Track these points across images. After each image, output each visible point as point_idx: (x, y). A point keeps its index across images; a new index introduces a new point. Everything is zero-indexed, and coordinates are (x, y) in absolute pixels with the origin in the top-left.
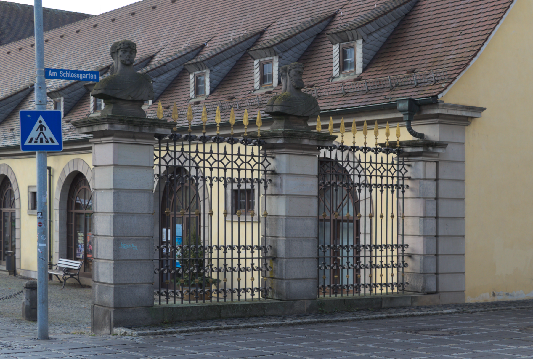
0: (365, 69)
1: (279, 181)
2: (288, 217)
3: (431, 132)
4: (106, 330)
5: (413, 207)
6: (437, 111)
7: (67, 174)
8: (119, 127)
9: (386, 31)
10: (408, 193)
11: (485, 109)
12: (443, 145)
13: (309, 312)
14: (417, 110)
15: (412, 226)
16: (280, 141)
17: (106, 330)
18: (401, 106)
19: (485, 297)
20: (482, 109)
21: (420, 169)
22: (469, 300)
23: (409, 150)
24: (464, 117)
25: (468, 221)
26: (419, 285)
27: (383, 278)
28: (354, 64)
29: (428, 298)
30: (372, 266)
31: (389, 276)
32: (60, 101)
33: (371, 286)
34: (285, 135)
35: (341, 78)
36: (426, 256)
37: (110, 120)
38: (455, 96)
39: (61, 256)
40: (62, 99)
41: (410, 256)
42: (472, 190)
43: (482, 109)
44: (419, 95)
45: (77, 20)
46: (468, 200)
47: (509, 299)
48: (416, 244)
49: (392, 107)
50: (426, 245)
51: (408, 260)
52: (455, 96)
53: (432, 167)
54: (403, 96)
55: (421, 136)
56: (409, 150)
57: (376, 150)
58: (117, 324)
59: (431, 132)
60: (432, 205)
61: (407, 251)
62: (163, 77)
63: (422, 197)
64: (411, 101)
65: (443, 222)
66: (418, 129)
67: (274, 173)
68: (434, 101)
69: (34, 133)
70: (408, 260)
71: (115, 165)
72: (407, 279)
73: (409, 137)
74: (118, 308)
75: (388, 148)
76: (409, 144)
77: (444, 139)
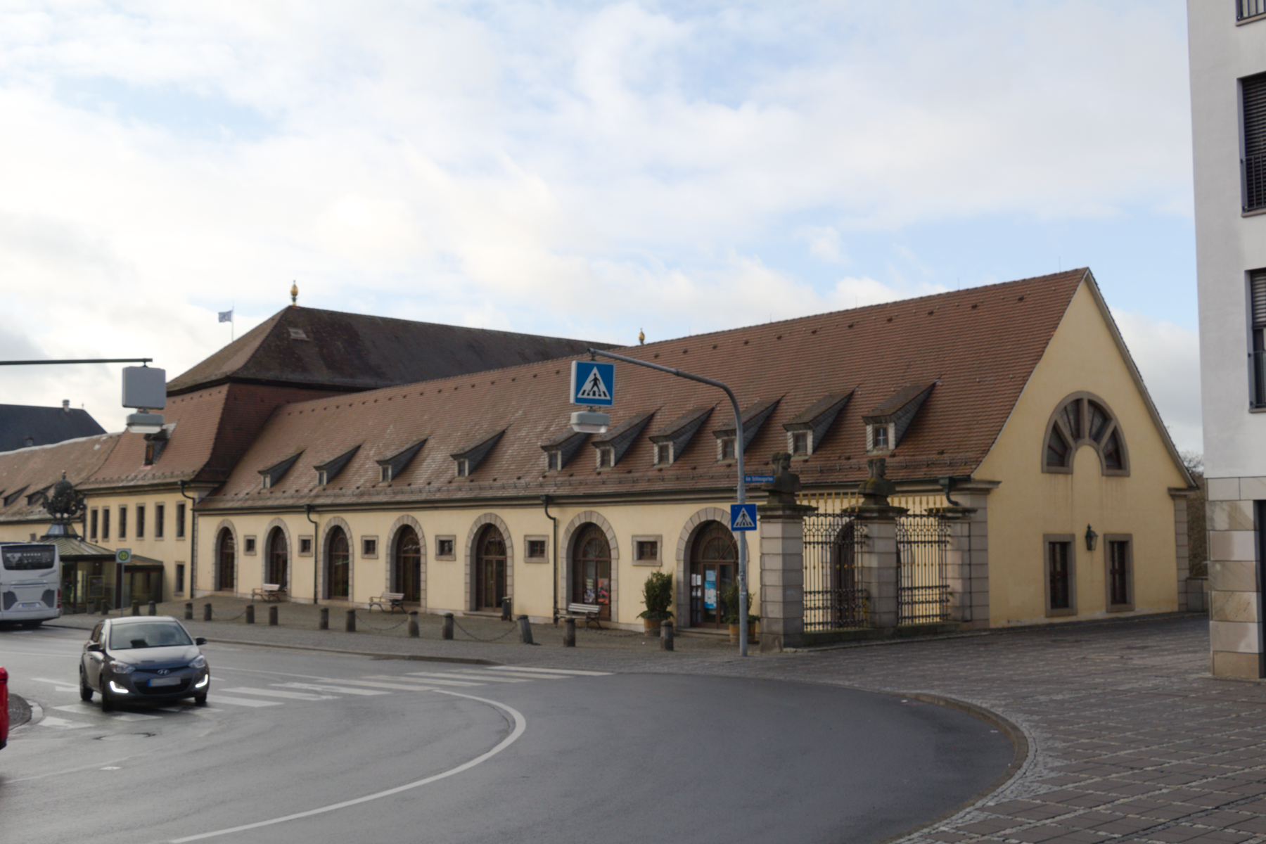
0: (897, 446)
1: (871, 543)
2: (879, 568)
3: (964, 500)
4: (777, 650)
5: (952, 557)
6: (969, 486)
7: (577, 524)
8: (788, 512)
9: (910, 415)
10: (949, 547)
11: (1089, 527)
12: (973, 511)
13: (893, 636)
14: (954, 485)
15: (951, 572)
16: (875, 515)
17: (777, 650)
18: (942, 481)
19: (1002, 623)
20: (998, 483)
21: (959, 528)
22: (992, 626)
23: (950, 515)
24: (986, 489)
25: (991, 566)
26: (958, 615)
27: (926, 610)
28: (886, 441)
29: (965, 626)
30: (913, 603)
31: (935, 609)
32: (556, 455)
33: (913, 617)
34: (879, 511)
35: (875, 453)
36: (964, 593)
37: (784, 509)
38: (980, 474)
39: (324, 598)
40: (559, 453)
41: (951, 594)
42: (994, 543)
43: (998, 483)
44: (959, 472)
45: (526, 360)
46: (990, 550)
47: (1019, 624)
48: (956, 585)
49: (935, 481)
50: (964, 586)
51: (950, 598)
52: (980, 474)
53: (966, 527)
54: (943, 474)
55: (956, 503)
56: (950, 515)
57: (922, 516)
58: (786, 645)
59: (964, 500)
60: (966, 556)
61: (949, 590)
62: (682, 439)
63: (957, 549)
64: (951, 479)
65: (974, 569)
66: (953, 498)
67: (866, 536)
68: (968, 479)
69: (739, 519)
70: (950, 598)
71: (783, 538)
72: (949, 611)
73: (946, 504)
74: (785, 635)
75: (931, 513)
76: (949, 510)
77: (975, 505)
